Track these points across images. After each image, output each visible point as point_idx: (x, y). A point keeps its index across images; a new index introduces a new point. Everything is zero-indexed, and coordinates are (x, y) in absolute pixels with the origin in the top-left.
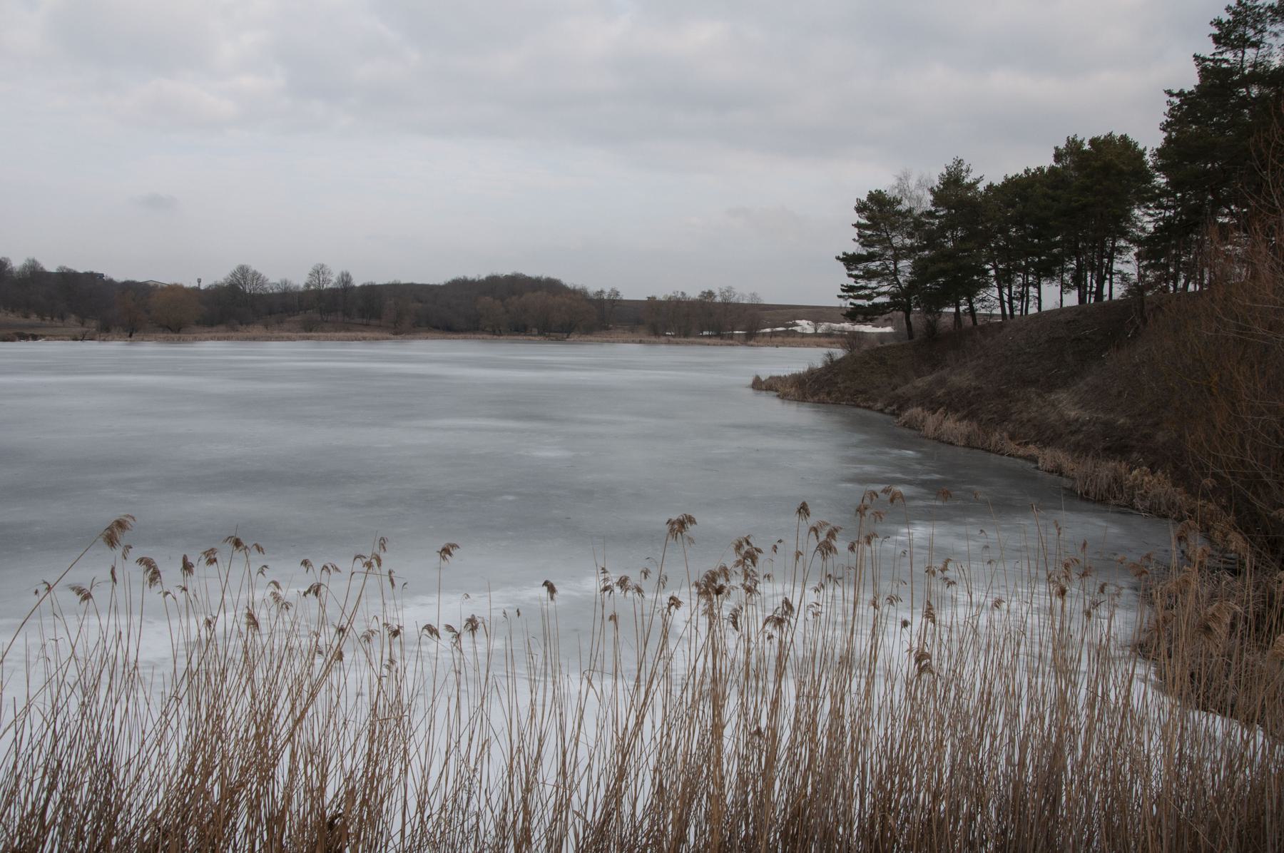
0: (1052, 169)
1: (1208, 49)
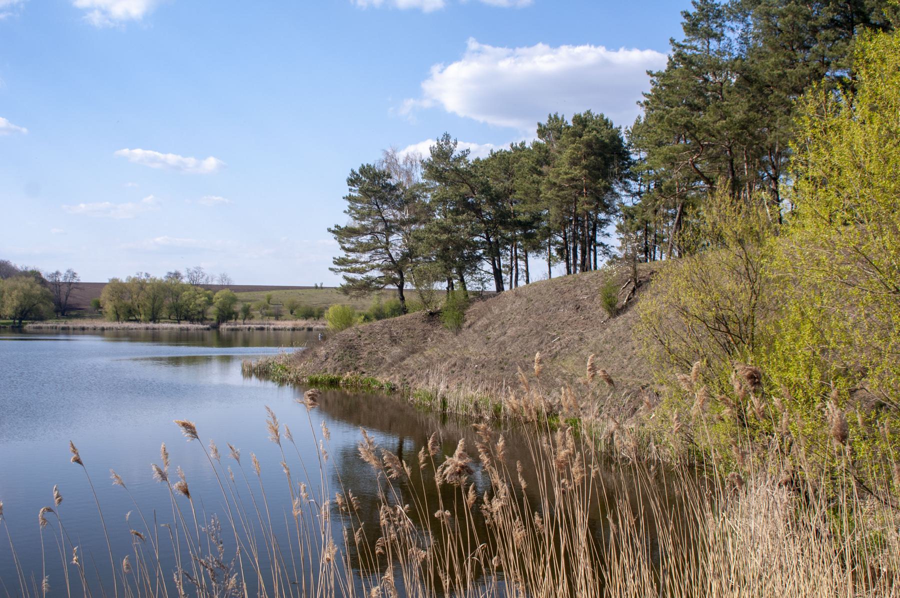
0: (537, 145)
1: (681, 36)
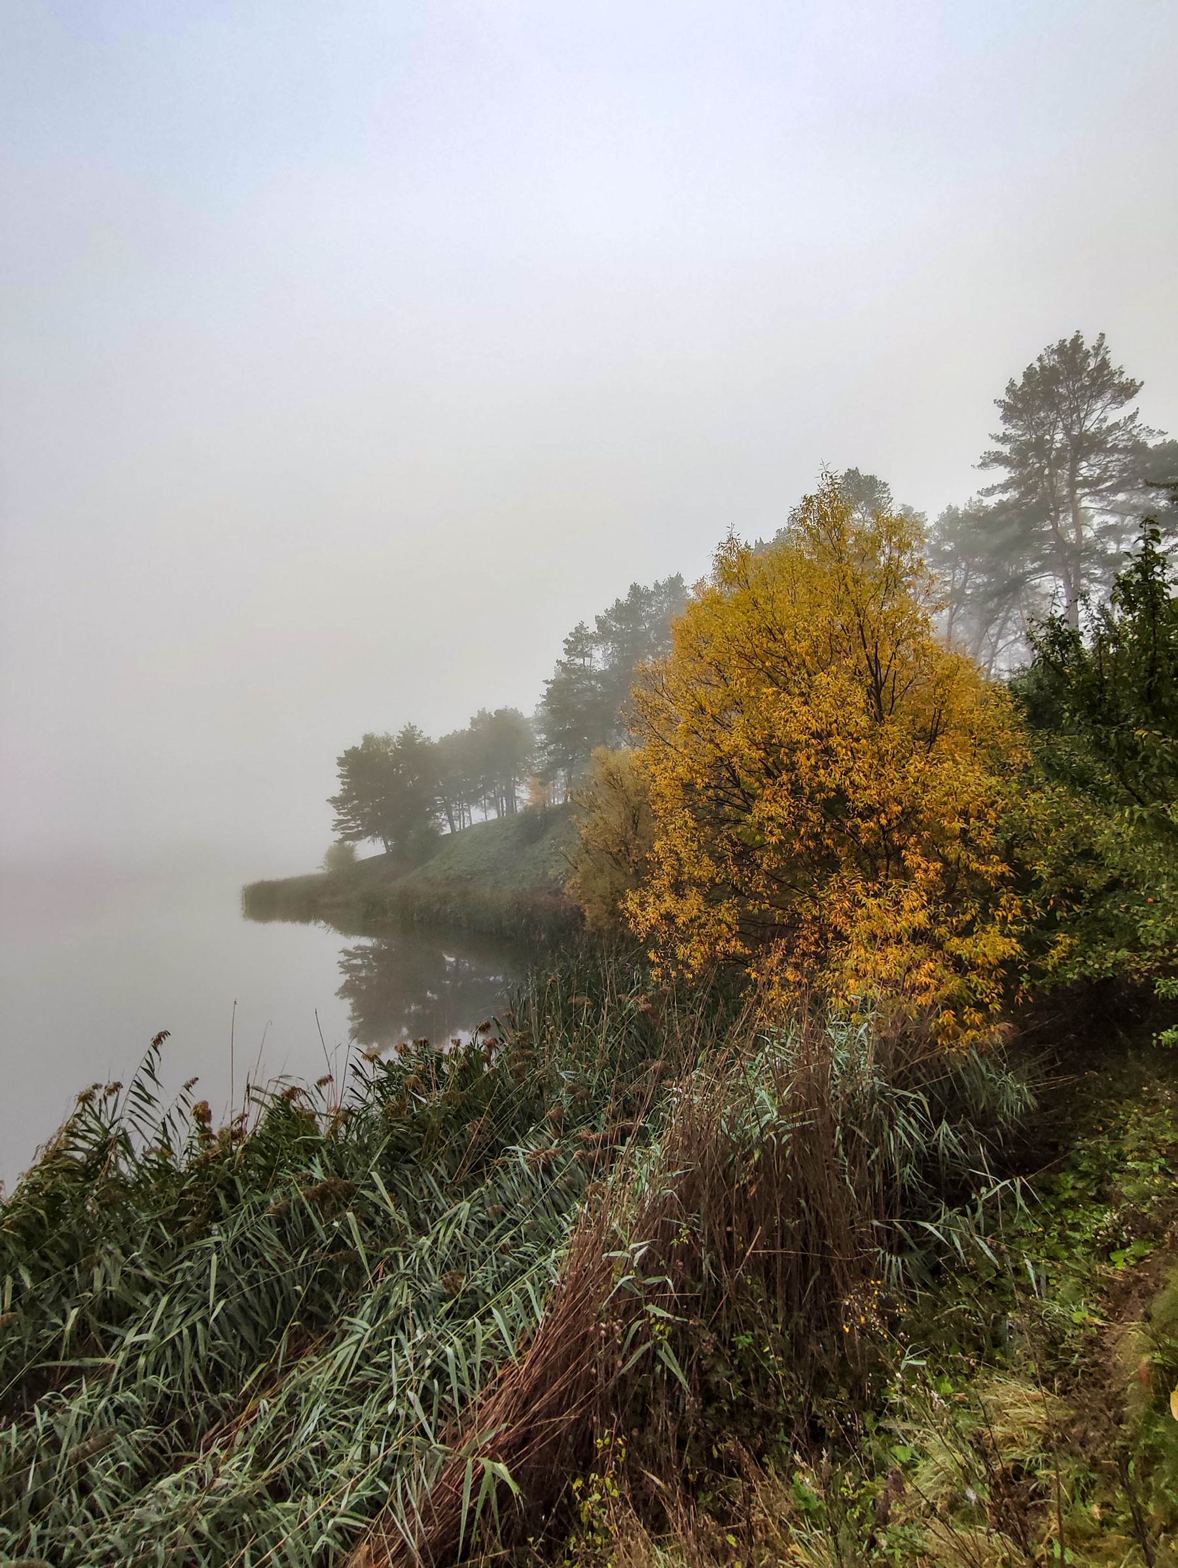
1: (565, 658)
